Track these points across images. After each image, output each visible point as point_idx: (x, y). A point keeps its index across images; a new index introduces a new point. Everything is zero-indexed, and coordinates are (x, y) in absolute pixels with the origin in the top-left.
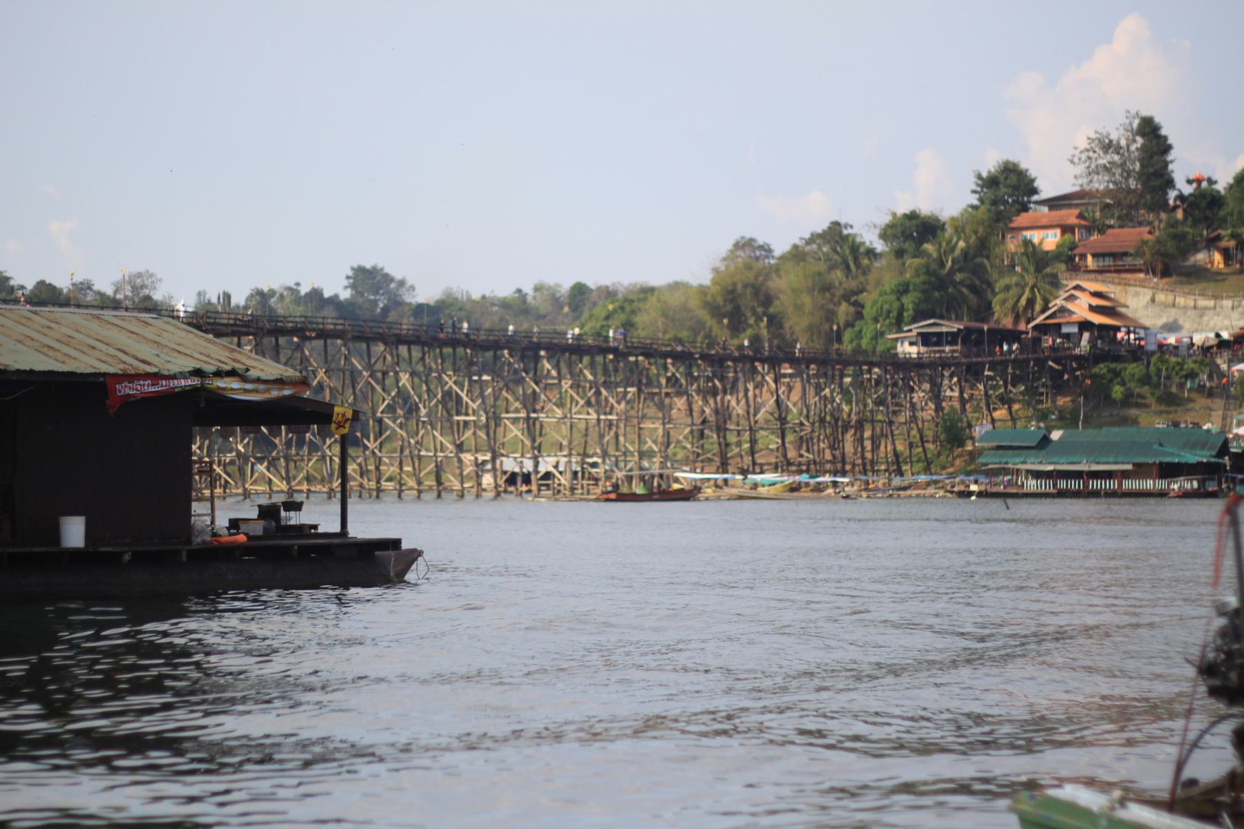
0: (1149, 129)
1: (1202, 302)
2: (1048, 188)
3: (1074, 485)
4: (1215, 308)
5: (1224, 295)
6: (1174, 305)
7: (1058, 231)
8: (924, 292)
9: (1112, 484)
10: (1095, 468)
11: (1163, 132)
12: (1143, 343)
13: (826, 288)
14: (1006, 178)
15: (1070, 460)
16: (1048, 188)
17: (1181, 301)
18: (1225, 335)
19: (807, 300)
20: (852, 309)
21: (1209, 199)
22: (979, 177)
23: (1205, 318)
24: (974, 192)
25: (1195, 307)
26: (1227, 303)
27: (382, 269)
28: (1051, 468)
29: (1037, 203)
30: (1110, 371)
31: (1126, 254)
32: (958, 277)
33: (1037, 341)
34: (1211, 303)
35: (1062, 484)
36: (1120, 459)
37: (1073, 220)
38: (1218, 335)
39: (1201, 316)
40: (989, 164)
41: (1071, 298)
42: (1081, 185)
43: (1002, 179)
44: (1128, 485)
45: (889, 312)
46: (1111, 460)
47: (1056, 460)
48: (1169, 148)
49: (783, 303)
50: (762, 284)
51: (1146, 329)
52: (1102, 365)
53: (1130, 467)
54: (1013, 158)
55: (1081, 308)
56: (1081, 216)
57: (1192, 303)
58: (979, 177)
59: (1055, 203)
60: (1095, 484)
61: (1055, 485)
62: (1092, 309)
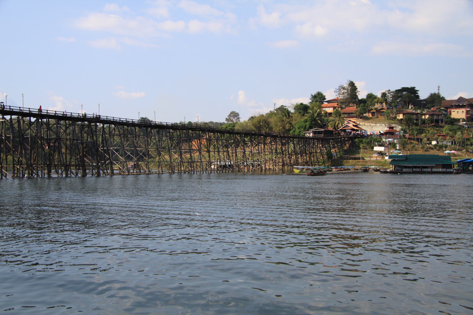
0: (352, 84)
1: (372, 125)
2: (328, 98)
3: (418, 170)
4: (375, 126)
5: (378, 123)
6: (365, 125)
7: (332, 108)
8: (311, 122)
9: (429, 170)
10: (424, 165)
11: (355, 85)
12: (364, 134)
13: (283, 121)
14: (319, 96)
15: (418, 163)
16: (328, 98)
17: (366, 124)
18: (382, 132)
19: (279, 124)
20: (290, 125)
21: (364, 101)
22: (312, 95)
23: (373, 128)
24: (310, 99)
25: (370, 126)
26: (379, 125)
27: (147, 118)
28: (411, 165)
29: (326, 102)
30: (359, 140)
31: (352, 113)
32: (317, 118)
33: (351, 133)
34: (374, 125)
35: (415, 170)
36: (432, 163)
37: (336, 106)
38: (380, 132)
39: (372, 128)
40: (314, 93)
41: (349, 123)
42: (337, 97)
43: (317, 96)
44: (434, 170)
45: (303, 126)
46: (429, 163)
47: (412, 163)
48: (357, 89)
49: (272, 125)
50: (267, 120)
51: (365, 130)
52: (357, 139)
53: (435, 165)
54: (320, 91)
55: (351, 125)
56: (337, 105)
57: (369, 125)
58: (312, 95)
59: (329, 102)
60: (425, 170)
61: (412, 170)
62: (354, 125)
